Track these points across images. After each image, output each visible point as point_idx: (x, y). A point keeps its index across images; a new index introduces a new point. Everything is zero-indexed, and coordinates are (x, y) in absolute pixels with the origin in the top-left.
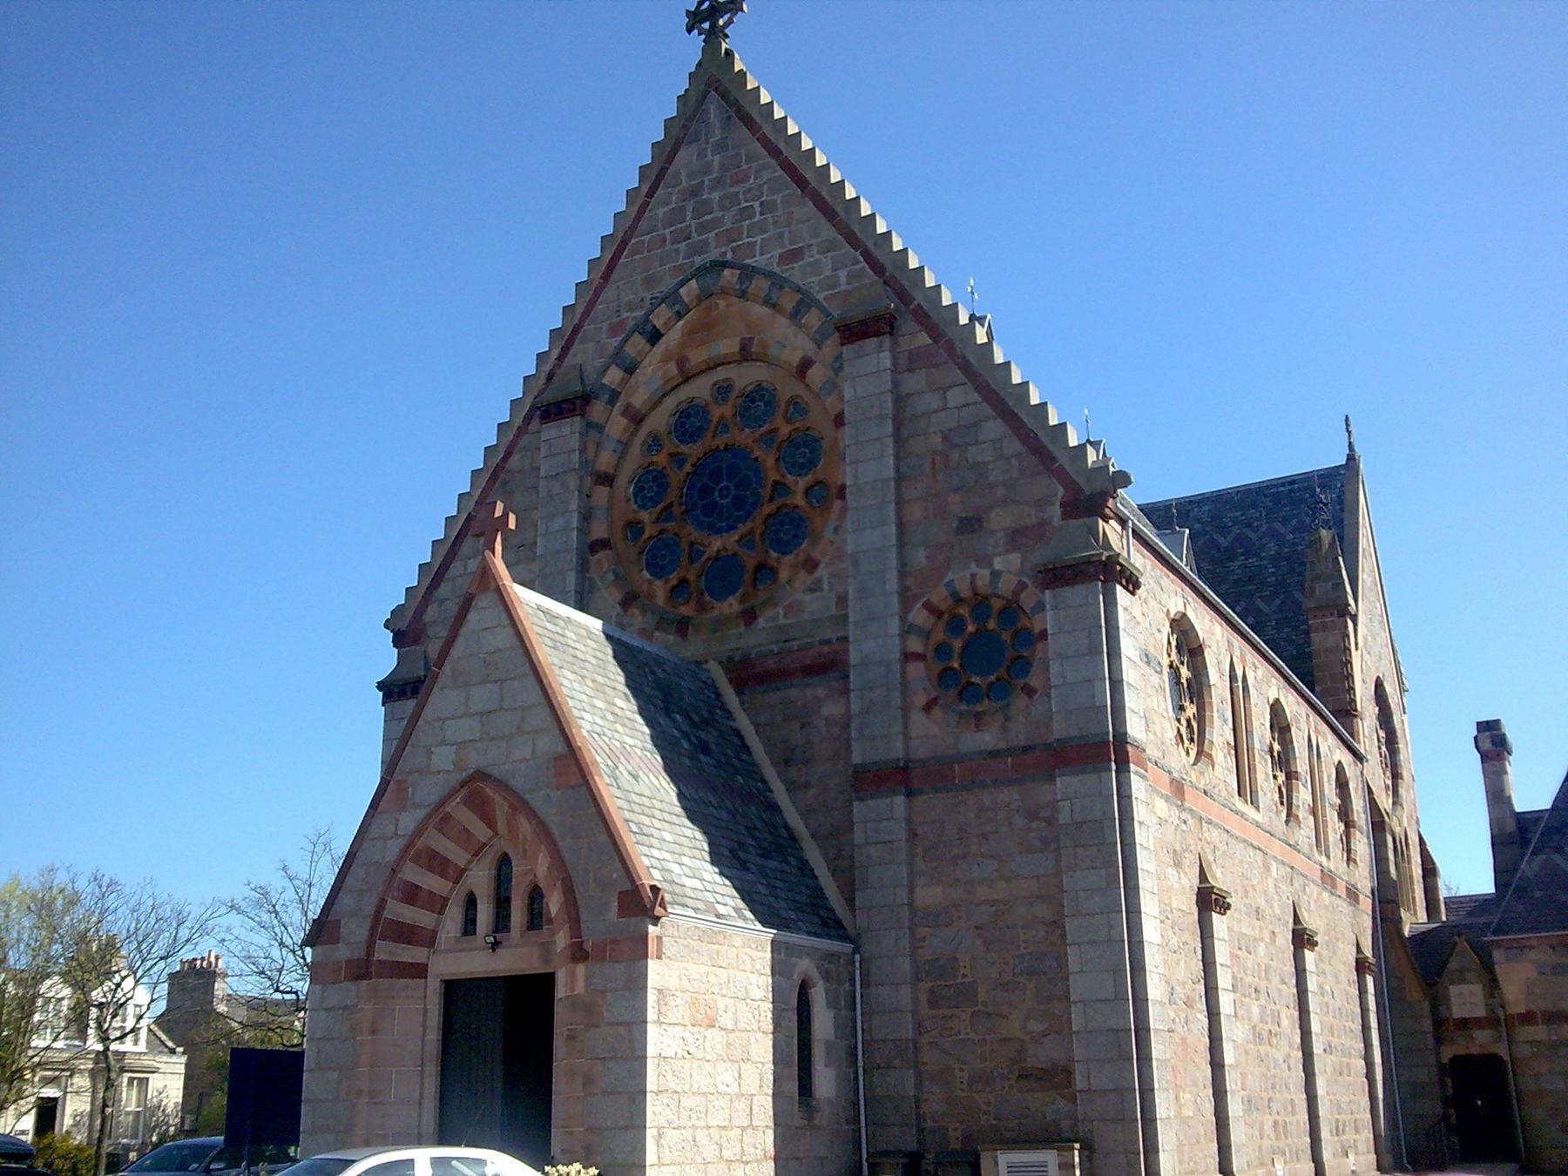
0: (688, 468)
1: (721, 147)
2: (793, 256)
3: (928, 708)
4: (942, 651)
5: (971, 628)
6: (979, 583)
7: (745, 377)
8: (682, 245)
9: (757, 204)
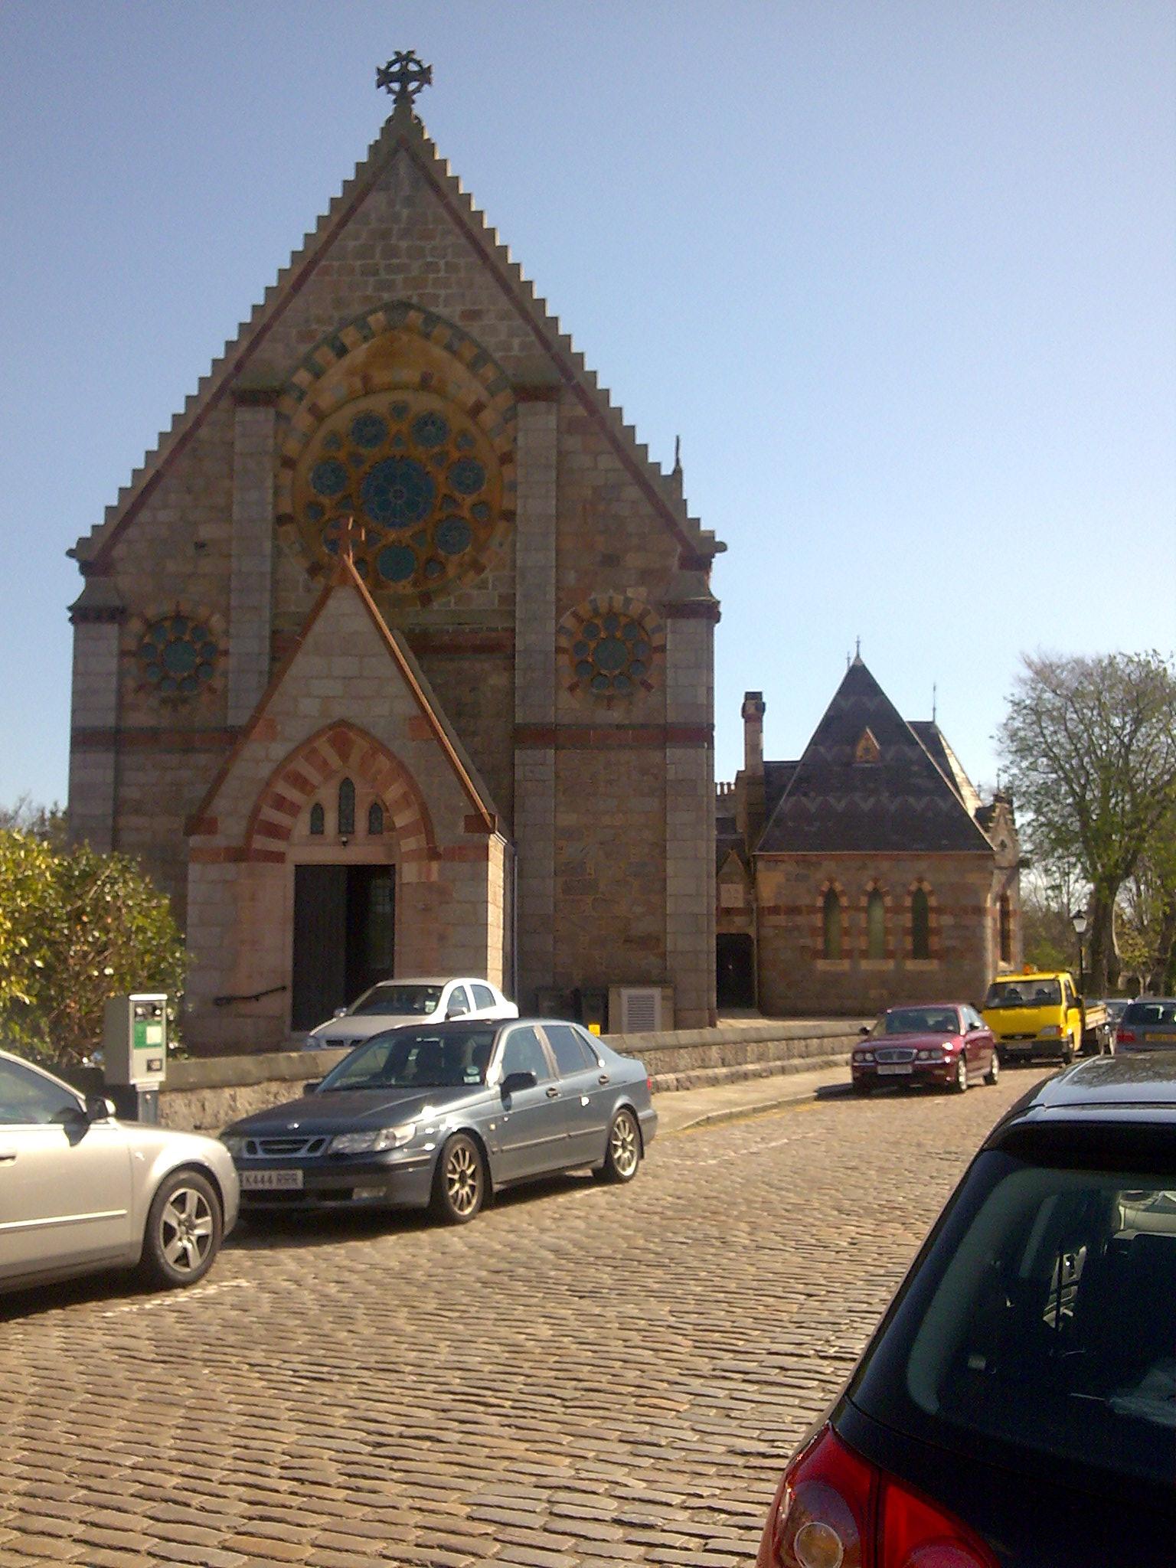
0: (366, 468)
1: (409, 202)
2: (472, 315)
3: (572, 689)
4: (579, 647)
5: (603, 635)
6: (615, 604)
7: (423, 403)
8: (372, 280)
9: (442, 263)
